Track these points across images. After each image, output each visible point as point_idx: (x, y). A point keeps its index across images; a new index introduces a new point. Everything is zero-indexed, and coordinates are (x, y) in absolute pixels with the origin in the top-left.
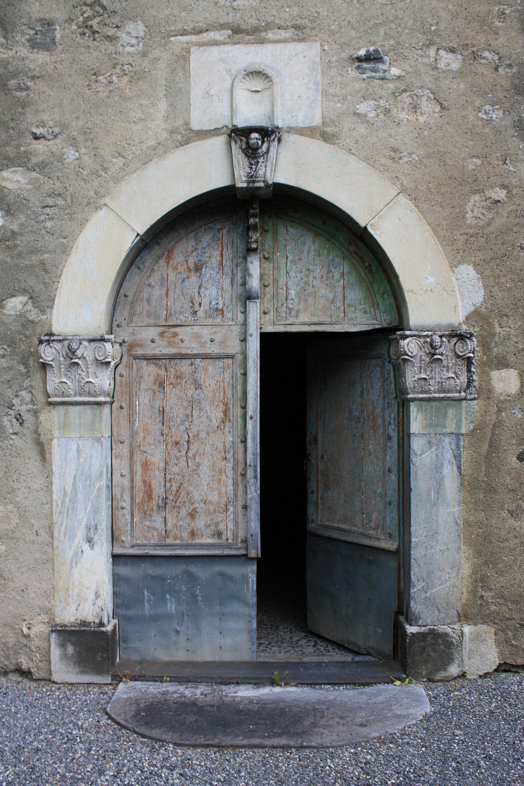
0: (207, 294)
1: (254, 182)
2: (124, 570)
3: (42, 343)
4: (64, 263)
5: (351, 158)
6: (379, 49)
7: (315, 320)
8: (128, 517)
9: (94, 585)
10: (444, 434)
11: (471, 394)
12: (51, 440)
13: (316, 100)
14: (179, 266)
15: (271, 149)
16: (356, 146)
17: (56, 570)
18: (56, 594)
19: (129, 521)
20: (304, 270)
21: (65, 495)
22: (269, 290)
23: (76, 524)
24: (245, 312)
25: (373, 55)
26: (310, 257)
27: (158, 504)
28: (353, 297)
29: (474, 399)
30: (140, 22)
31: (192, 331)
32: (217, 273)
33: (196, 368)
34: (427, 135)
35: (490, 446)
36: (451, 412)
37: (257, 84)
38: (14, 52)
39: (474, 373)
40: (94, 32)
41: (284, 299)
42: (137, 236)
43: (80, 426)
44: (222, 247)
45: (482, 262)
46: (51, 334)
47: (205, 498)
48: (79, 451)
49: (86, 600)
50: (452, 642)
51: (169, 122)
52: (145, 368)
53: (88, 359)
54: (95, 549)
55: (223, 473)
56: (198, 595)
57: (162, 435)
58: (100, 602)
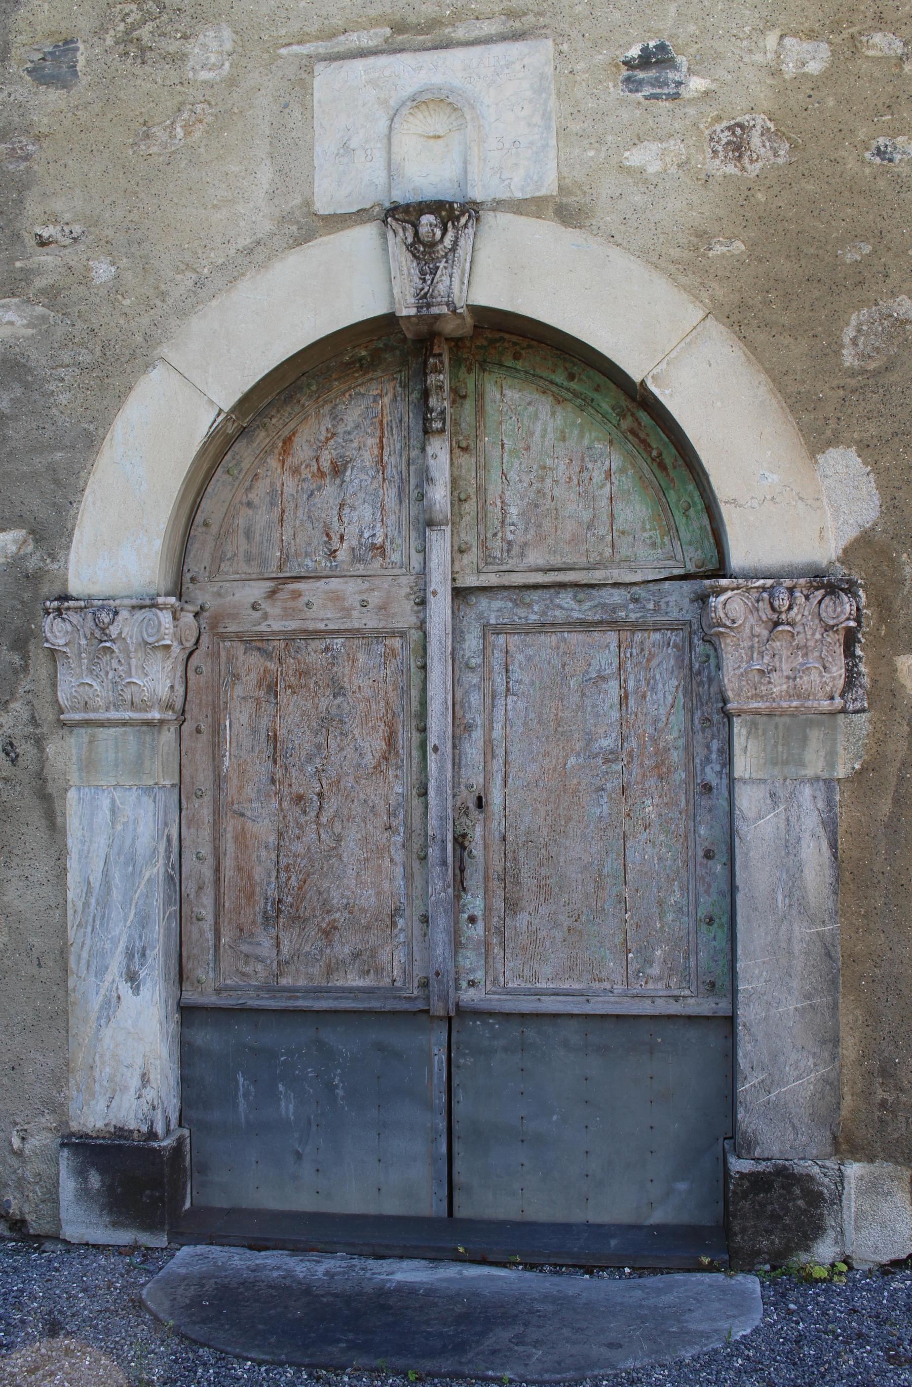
0: (355, 519)
1: (429, 306)
2: (203, 1037)
3: (49, 614)
4: (89, 466)
5: (615, 253)
6: (667, 43)
7: (556, 561)
8: (210, 935)
9: (139, 1061)
10: (803, 781)
11: (856, 699)
12: (66, 790)
13: (545, 146)
14: (303, 466)
15: (462, 242)
16: (623, 228)
17: (73, 1031)
18: (71, 1075)
19: (211, 943)
20: (535, 467)
21: (89, 892)
22: (470, 507)
23: (108, 946)
24: (423, 551)
25: (654, 54)
26: (546, 443)
27: (265, 912)
28: (630, 517)
29: (862, 710)
30: (224, 25)
31: (327, 587)
32: (374, 478)
33: (334, 657)
34: (763, 200)
35: (896, 801)
36: (815, 736)
37: (437, 122)
38: (6, 93)
39: (860, 658)
40: (143, 50)
41: (497, 523)
42: (218, 415)
43: (116, 766)
44: (382, 429)
45: (875, 441)
46: (66, 598)
47: (351, 901)
48: (114, 811)
49: (125, 1089)
50: (822, 1193)
51: (276, 201)
52: (241, 658)
53: (129, 641)
54: (141, 993)
55: (386, 855)
56: (337, 1086)
57: (273, 781)
58: (150, 1094)
